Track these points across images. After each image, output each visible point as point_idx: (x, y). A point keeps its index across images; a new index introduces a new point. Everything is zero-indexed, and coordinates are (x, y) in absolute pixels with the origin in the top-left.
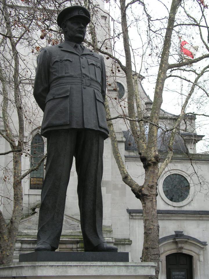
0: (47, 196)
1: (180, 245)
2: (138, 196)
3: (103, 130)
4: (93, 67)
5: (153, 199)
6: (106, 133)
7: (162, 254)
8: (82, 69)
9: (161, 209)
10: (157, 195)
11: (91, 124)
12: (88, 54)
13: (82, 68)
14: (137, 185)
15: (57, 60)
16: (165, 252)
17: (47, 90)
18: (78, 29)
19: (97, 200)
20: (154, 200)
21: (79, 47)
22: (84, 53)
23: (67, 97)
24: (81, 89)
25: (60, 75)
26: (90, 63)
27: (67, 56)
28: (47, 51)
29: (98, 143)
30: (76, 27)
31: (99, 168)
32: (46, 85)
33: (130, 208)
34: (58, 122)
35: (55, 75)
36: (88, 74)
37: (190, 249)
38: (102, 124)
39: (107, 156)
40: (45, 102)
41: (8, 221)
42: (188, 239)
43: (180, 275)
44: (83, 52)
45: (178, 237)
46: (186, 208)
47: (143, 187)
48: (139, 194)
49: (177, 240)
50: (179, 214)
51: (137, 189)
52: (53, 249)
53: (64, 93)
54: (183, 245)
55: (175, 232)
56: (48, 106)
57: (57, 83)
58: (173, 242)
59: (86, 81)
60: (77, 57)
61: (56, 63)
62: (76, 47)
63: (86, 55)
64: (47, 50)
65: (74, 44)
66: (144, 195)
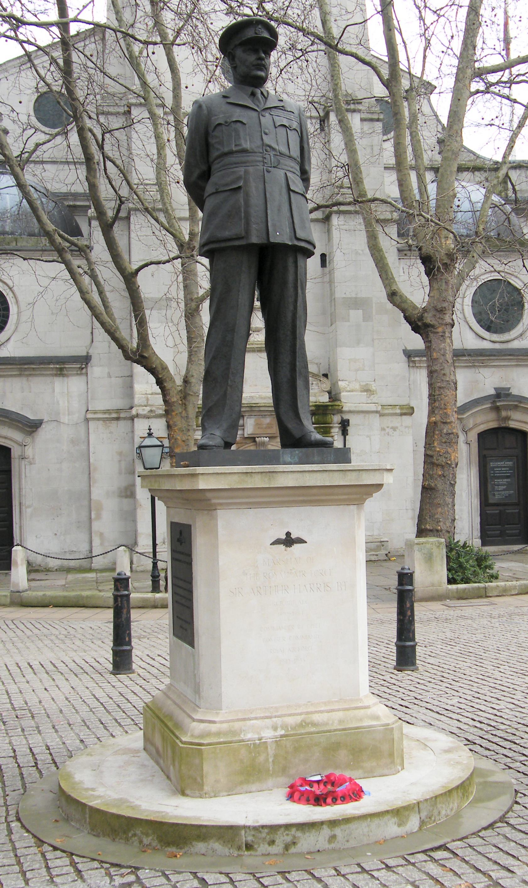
0: (214, 358)
1: (504, 414)
2: (416, 329)
3: (303, 244)
4: (283, 130)
5: (444, 332)
6: (310, 247)
7: (470, 429)
8: (264, 137)
9: (469, 348)
10: (453, 326)
11: (280, 235)
12: (275, 107)
13: (263, 135)
14: (415, 307)
15: (220, 122)
16: (475, 425)
17: (206, 175)
18: (255, 63)
19: (298, 363)
20: (447, 334)
21: (259, 95)
22: (269, 105)
23: (239, 188)
24: (262, 174)
25: (226, 150)
26: (278, 124)
27: (238, 114)
28: (204, 107)
29: (296, 267)
30: (252, 58)
31: (299, 308)
32: (204, 167)
33: (409, 348)
34: (227, 234)
35: (218, 149)
36: (274, 145)
37: (525, 420)
38: (300, 234)
39: (362, 251)
40: (203, 196)
41: (179, 381)
42: (521, 402)
43: (504, 467)
44: (265, 104)
45: (501, 398)
46: (516, 345)
47: (425, 310)
48: (418, 325)
49: (498, 404)
50: (505, 355)
51: (415, 314)
52: (228, 445)
53: (233, 182)
54: (510, 413)
55: (495, 389)
56: (209, 203)
57: (221, 164)
58: (491, 408)
59: (271, 157)
60: (254, 114)
61: (219, 128)
62: (253, 94)
63: (270, 108)
64: (202, 103)
65: (250, 89)
66: (427, 326)
